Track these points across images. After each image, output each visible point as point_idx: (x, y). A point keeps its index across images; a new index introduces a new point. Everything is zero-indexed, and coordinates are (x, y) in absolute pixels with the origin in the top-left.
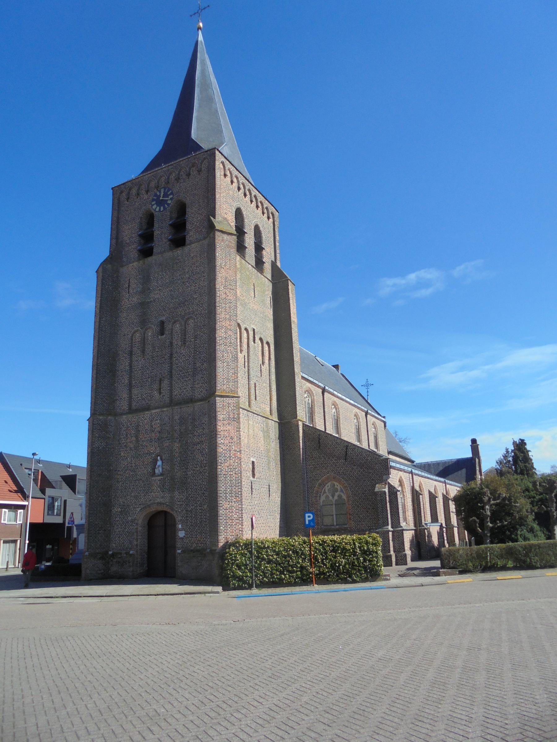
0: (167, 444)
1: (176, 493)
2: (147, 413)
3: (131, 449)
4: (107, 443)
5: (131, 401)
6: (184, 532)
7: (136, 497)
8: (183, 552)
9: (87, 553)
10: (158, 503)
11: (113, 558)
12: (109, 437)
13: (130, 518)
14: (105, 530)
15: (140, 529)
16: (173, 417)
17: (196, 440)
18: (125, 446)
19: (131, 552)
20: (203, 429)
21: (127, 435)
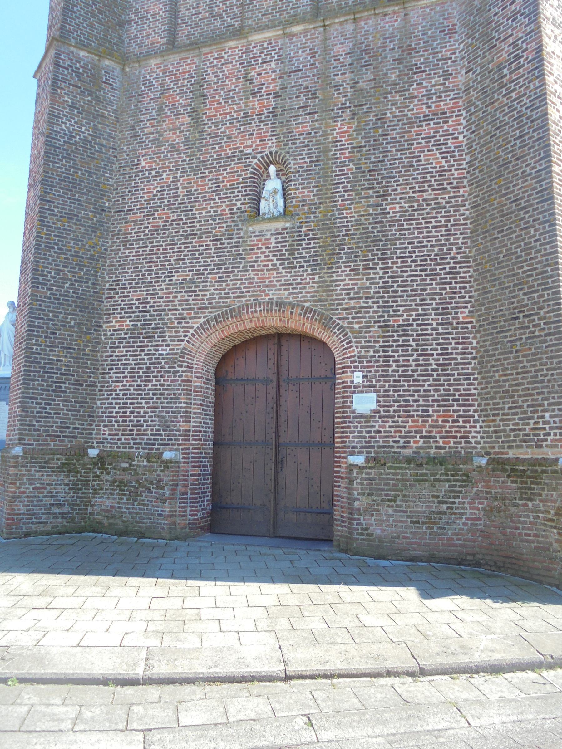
0: (304, 124)
1: (344, 276)
2: (232, 44)
3: (174, 148)
4: (95, 128)
5: (176, 24)
6: (374, 396)
7: (190, 288)
8: (376, 461)
9: (18, 450)
10: (270, 303)
11: (102, 468)
12: (103, 116)
13: (164, 351)
14: (78, 383)
15: (197, 383)
16: (326, 50)
17: (416, 108)
18: (153, 141)
19: (168, 455)
20: (446, 75)
21: (161, 110)
